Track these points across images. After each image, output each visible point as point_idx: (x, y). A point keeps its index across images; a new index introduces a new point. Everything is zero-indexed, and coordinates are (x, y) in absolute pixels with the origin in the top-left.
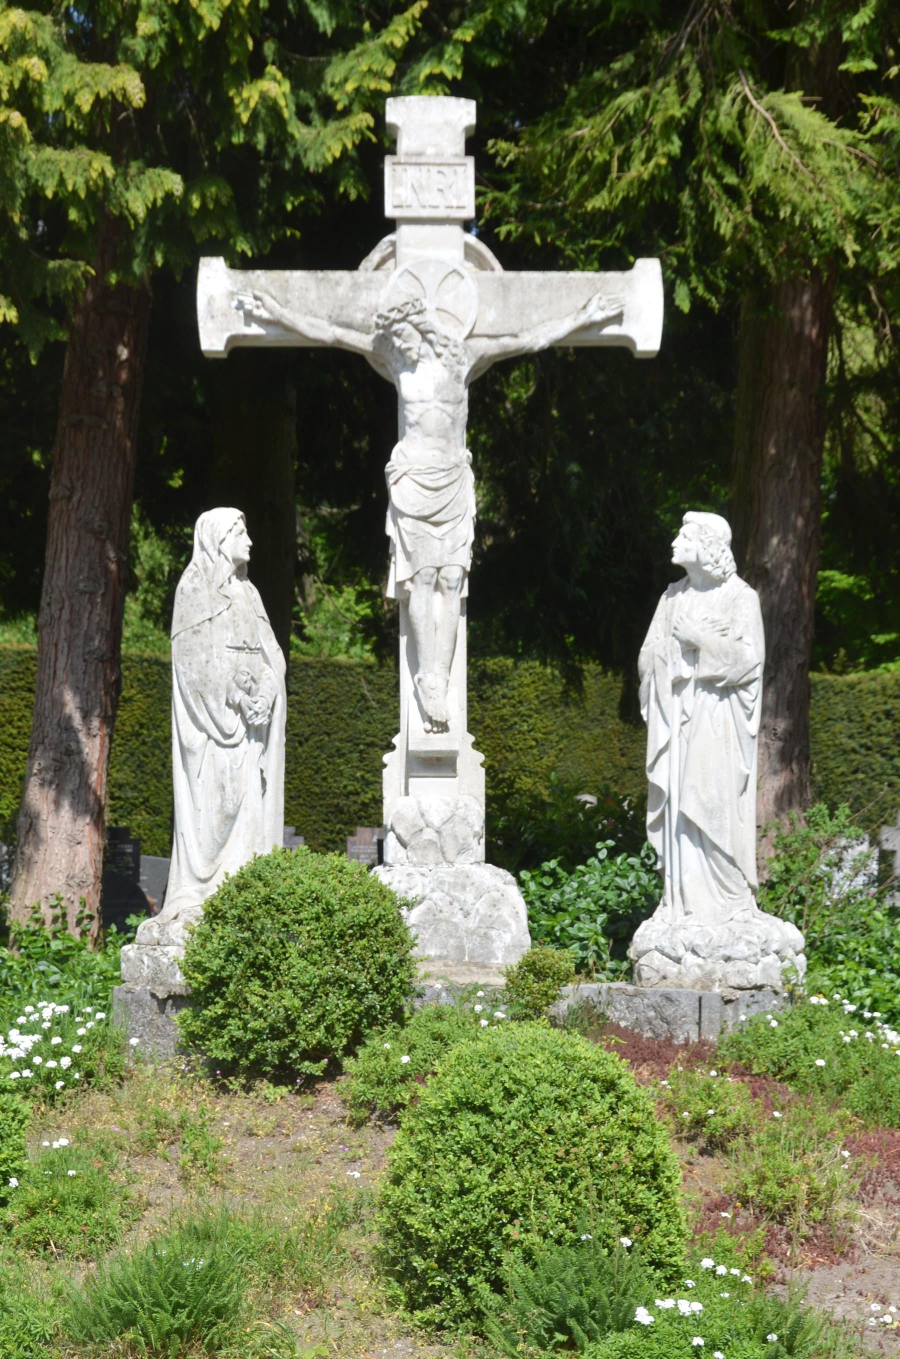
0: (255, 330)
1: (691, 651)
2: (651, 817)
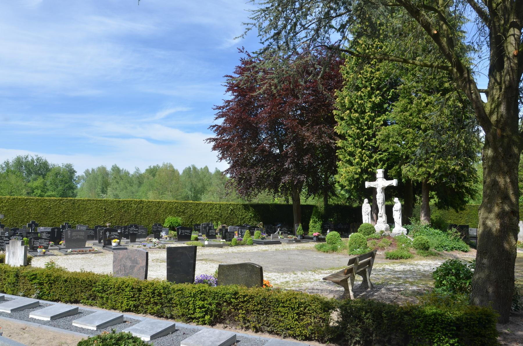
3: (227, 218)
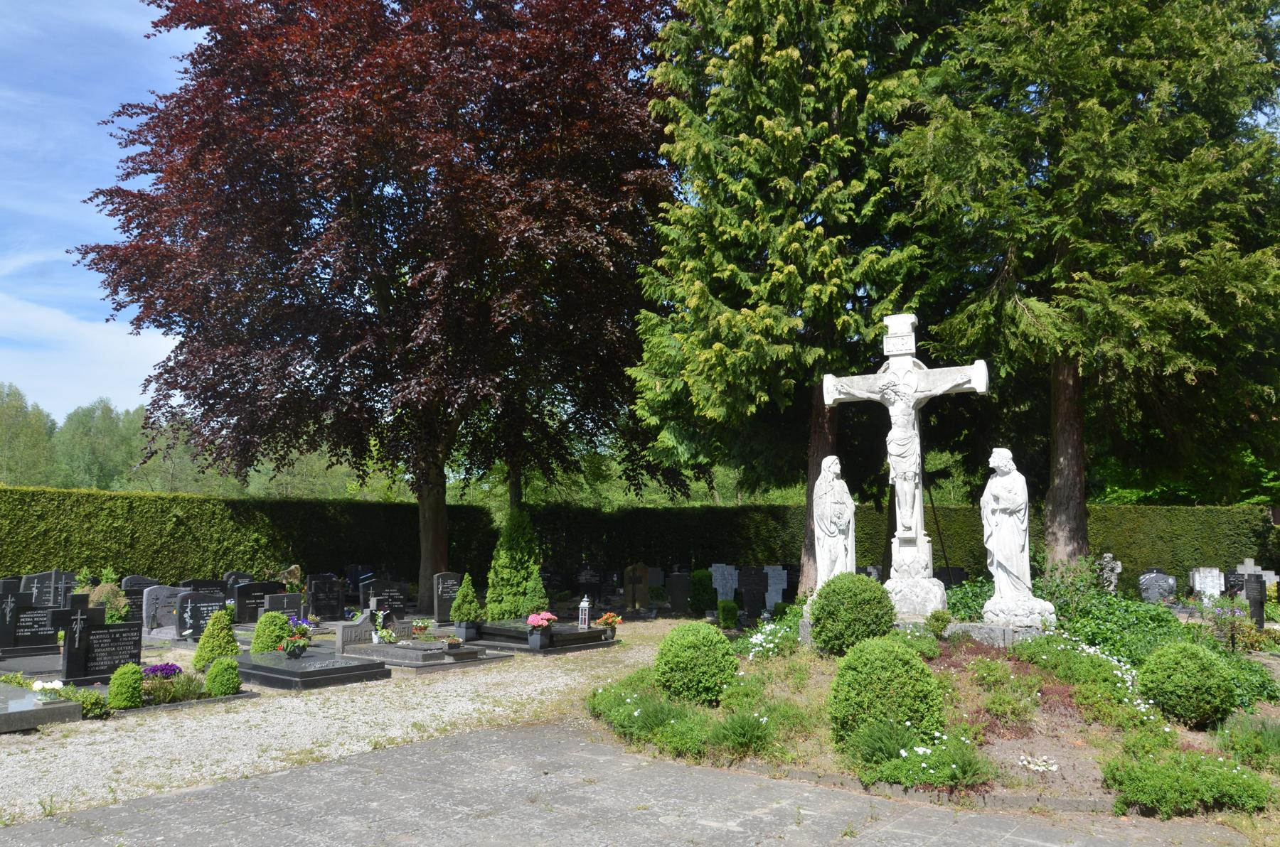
0: (842, 396)
1: (996, 499)
2: (989, 561)
3: (157, 552)
